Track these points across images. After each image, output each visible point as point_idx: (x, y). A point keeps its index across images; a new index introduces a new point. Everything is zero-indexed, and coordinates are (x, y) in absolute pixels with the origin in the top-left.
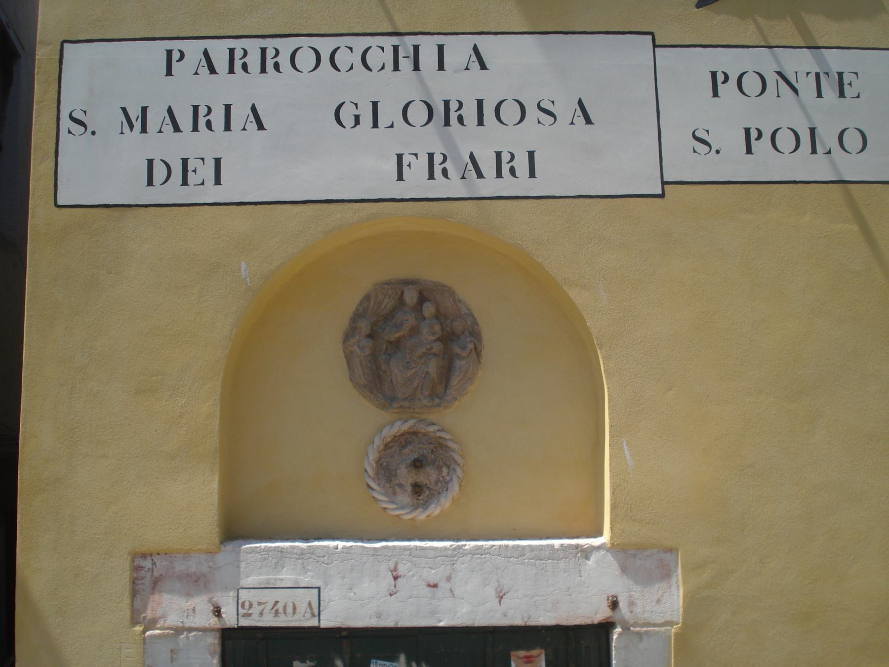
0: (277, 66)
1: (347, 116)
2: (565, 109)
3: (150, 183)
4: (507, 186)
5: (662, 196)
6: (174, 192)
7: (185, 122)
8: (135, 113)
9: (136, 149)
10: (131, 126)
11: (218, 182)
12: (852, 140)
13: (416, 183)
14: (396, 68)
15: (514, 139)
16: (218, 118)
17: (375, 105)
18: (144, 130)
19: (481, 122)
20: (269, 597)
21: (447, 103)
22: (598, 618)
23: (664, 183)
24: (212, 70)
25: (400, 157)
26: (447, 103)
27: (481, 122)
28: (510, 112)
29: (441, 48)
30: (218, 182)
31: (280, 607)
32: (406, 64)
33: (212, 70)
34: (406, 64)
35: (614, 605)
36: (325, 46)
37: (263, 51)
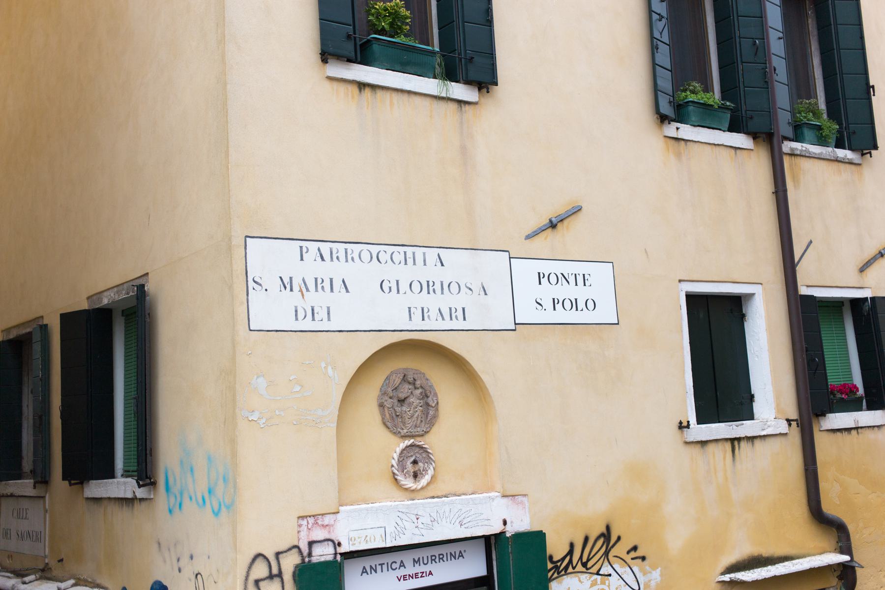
0: (353, 259)
1: (386, 286)
2: (476, 288)
3: (297, 319)
4: (455, 325)
5: (514, 330)
6: (308, 324)
7: (311, 286)
8: (286, 280)
9: (293, 299)
10: (285, 288)
11: (329, 319)
12: (590, 305)
13: (417, 323)
14: (406, 264)
15: (458, 301)
16: (327, 285)
17: (397, 282)
18: (291, 290)
19: (442, 293)
20: (363, 533)
21: (428, 282)
22: (497, 531)
23: (516, 324)
24: (323, 259)
25: (410, 308)
26: (428, 282)
27: (442, 293)
28: (454, 287)
29: (424, 254)
30: (329, 319)
31: (368, 538)
32: (410, 261)
33: (323, 259)
34: (410, 261)
35: (505, 523)
36: (374, 249)
37: (346, 250)
